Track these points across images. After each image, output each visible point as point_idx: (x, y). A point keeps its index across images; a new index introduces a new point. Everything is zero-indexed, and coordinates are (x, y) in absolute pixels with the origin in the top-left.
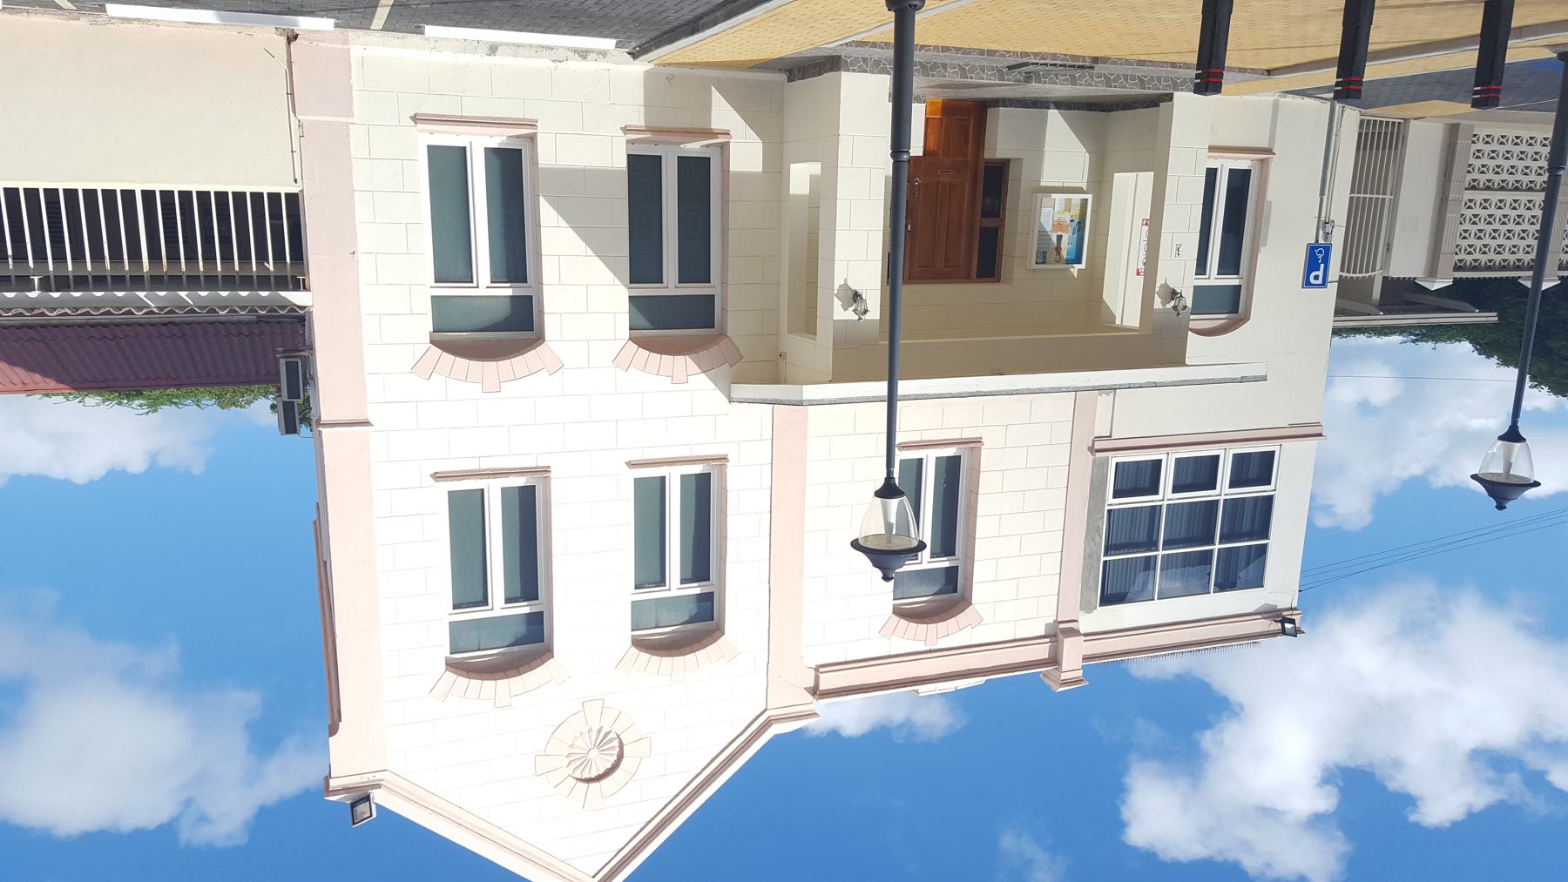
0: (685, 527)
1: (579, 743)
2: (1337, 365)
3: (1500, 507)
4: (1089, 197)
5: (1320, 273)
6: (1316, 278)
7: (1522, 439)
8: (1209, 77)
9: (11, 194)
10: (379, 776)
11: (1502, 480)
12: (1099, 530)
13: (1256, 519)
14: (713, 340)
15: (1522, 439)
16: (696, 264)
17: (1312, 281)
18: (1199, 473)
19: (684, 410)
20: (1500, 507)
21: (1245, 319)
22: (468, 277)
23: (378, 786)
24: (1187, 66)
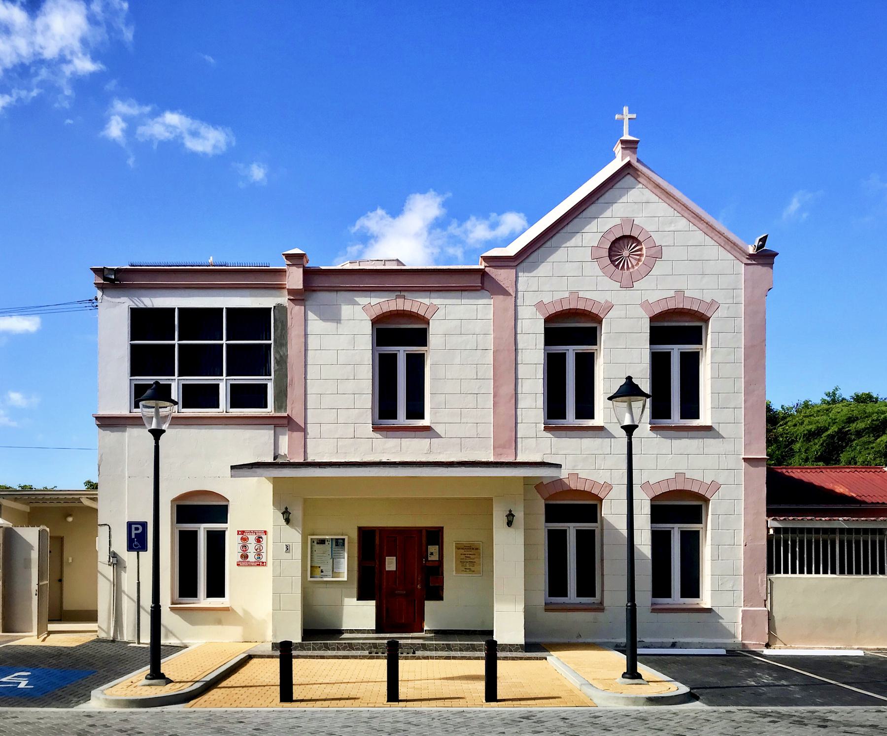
0: (568, 393)
1: (634, 262)
2: (716, 486)
3: (629, 379)
4: (309, 579)
5: (134, 532)
6: (137, 529)
7: (623, 427)
8: (285, 652)
9: (882, 572)
10: (749, 262)
11: (632, 398)
12: (277, 362)
13: (140, 361)
14: (552, 497)
15: (623, 427)
16: (556, 541)
17: (140, 527)
18: (202, 397)
19: (585, 461)
20: (629, 379)
21: (173, 501)
22: (579, 533)
23: (751, 255)
24: (298, 657)
